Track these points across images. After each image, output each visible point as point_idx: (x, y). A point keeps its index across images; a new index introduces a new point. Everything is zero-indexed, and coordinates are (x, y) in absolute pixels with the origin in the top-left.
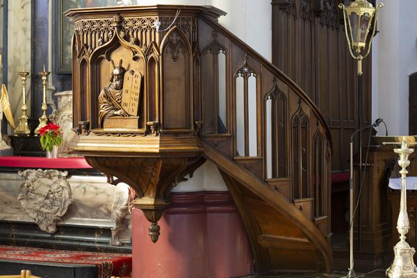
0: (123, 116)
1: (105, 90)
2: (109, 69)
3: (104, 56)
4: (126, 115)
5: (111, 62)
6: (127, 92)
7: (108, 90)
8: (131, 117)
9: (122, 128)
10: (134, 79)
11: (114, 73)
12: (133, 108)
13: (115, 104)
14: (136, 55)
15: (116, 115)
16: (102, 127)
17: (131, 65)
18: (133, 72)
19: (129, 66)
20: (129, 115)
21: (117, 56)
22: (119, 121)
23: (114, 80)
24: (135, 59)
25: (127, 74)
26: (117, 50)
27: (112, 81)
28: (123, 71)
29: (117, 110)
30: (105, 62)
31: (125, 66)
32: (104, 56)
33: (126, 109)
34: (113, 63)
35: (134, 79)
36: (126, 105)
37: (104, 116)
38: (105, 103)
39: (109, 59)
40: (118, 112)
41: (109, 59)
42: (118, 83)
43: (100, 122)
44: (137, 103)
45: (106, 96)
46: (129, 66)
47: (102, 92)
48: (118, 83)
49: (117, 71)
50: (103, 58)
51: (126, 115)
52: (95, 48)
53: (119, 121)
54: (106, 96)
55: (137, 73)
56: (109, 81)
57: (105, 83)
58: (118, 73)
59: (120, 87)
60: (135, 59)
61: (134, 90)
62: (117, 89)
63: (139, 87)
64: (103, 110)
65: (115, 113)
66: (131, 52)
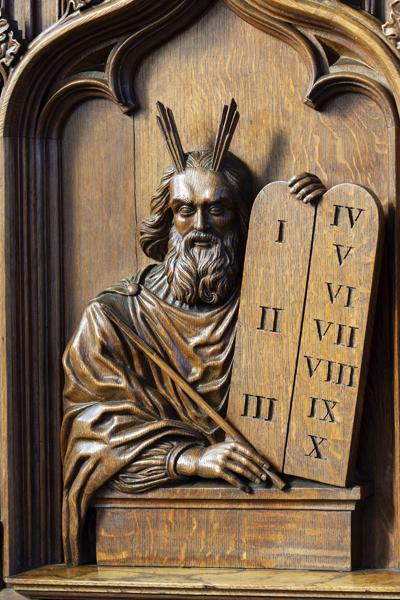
0: (244, 481)
1: (114, 310)
2: (133, 165)
3: (104, 78)
4: (264, 481)
5: (148, 126)
6: (270, 319)
7: (135, 309)
8: (298, 492)
9: (233, 563)
10: (328, 235)
11: (181, 192)
12: (317, 428)
13: (181, 405)
14: (335, 71)
15: (196, 478)
16: (88, 559)
17: (295, 140)
18: (313, 188)
19: (279, 146)
20: (289, 480)
21: (191, 81)
22: (205, 525)
23: (177, 241)
24: (329, 96)
25: (274, 203)
26: (189, 40)
27: (157, 247)
28: (239, 188)
29: (198, 441)
30: (103, 123)
31: (249, 148)
32: (104, 78)
33: (267, 436)
34: (167, 120)
35: (328, 235)
36: (263, 408)
37: (108, 484)
38: (109, 394)
39: (134, 106)
40: (211, 460)
41: (134, 106)
42: (206, 259)
43: (71, 526)
44: (347, 398)
45: (155, 265)
46: (279, 146)
47: (91, 325)
48: (206, 259)
49: (195, 184)
50: (88, 95)
51: (264, 481)
52: (36, 28)
53: (214, 516)
54: (125, 348)
55: (344, 191)
56: (134, 243)
57: (102, 263)
58: (207, 194)
59: (221, 291)
60: (329, 96)
61: (321, 309)
62: (198, 302)
63: (364, 291)
64: (95, 442)
65: (187, 463)
66: (228, 415)
